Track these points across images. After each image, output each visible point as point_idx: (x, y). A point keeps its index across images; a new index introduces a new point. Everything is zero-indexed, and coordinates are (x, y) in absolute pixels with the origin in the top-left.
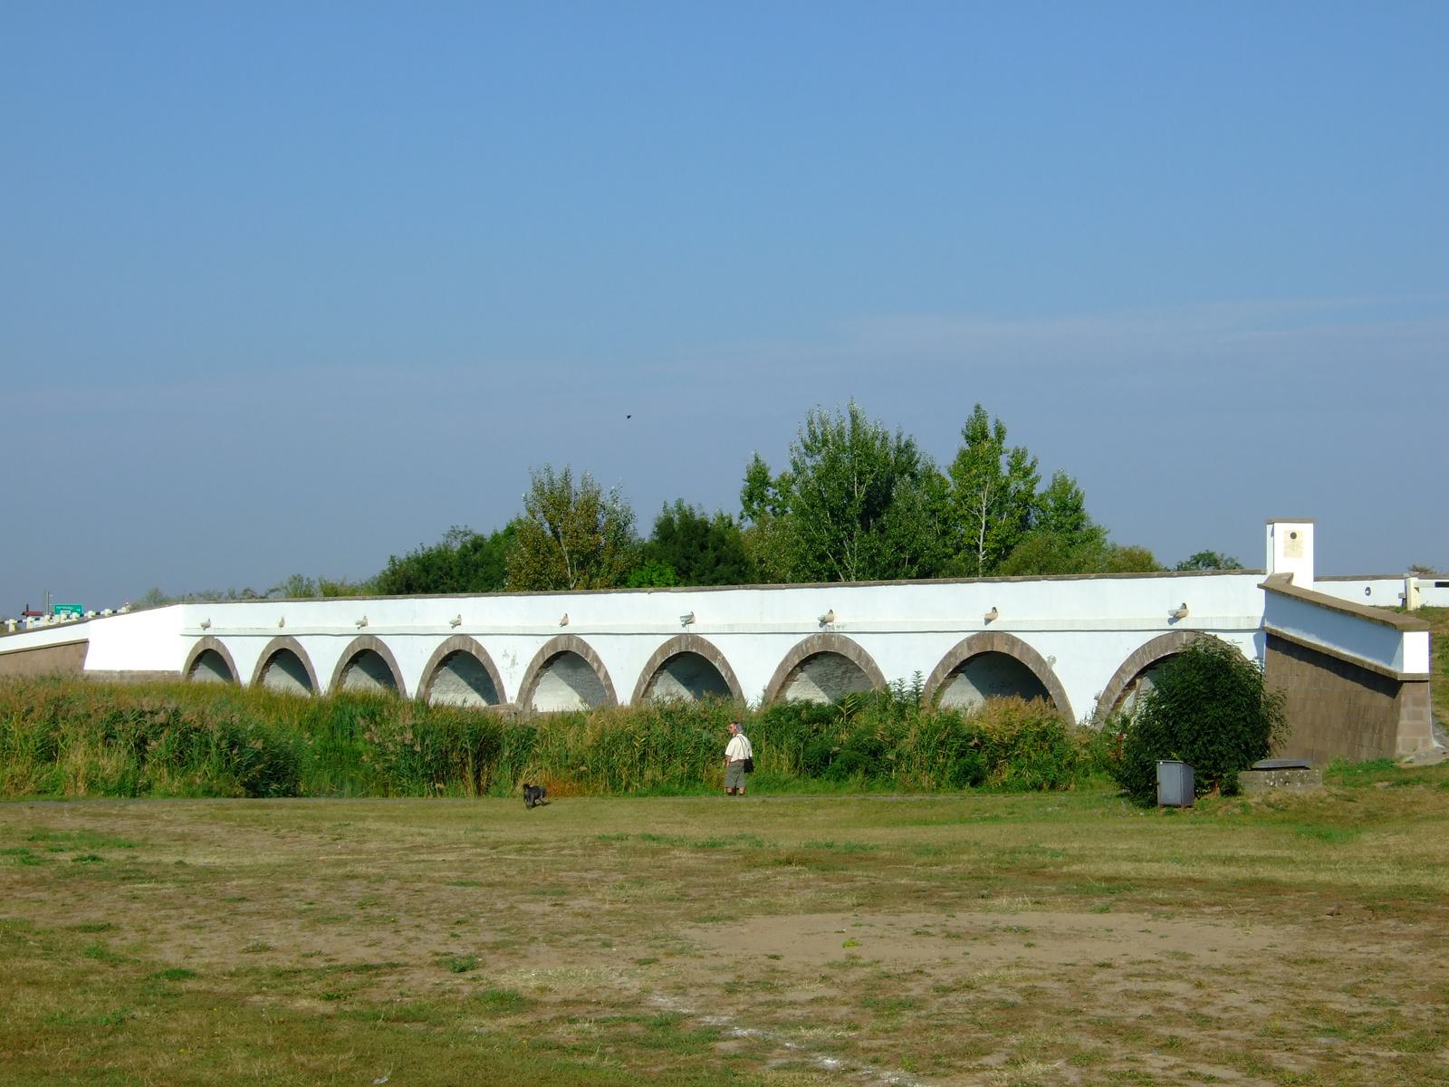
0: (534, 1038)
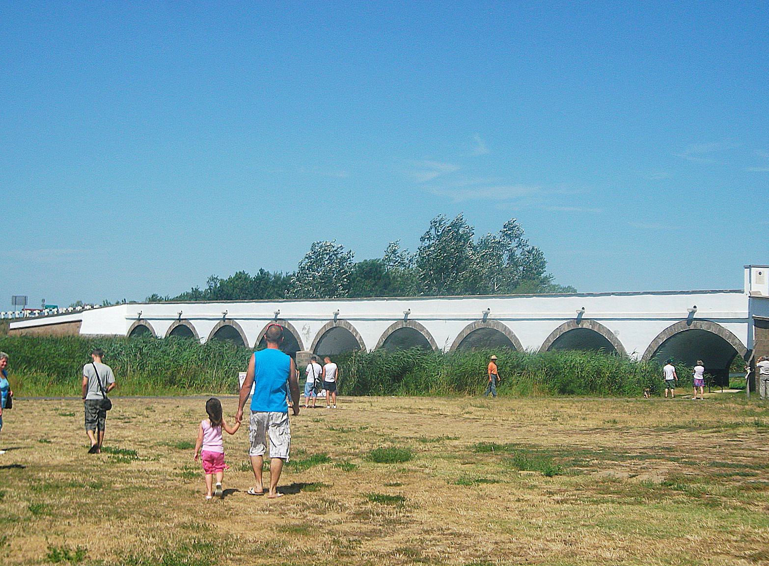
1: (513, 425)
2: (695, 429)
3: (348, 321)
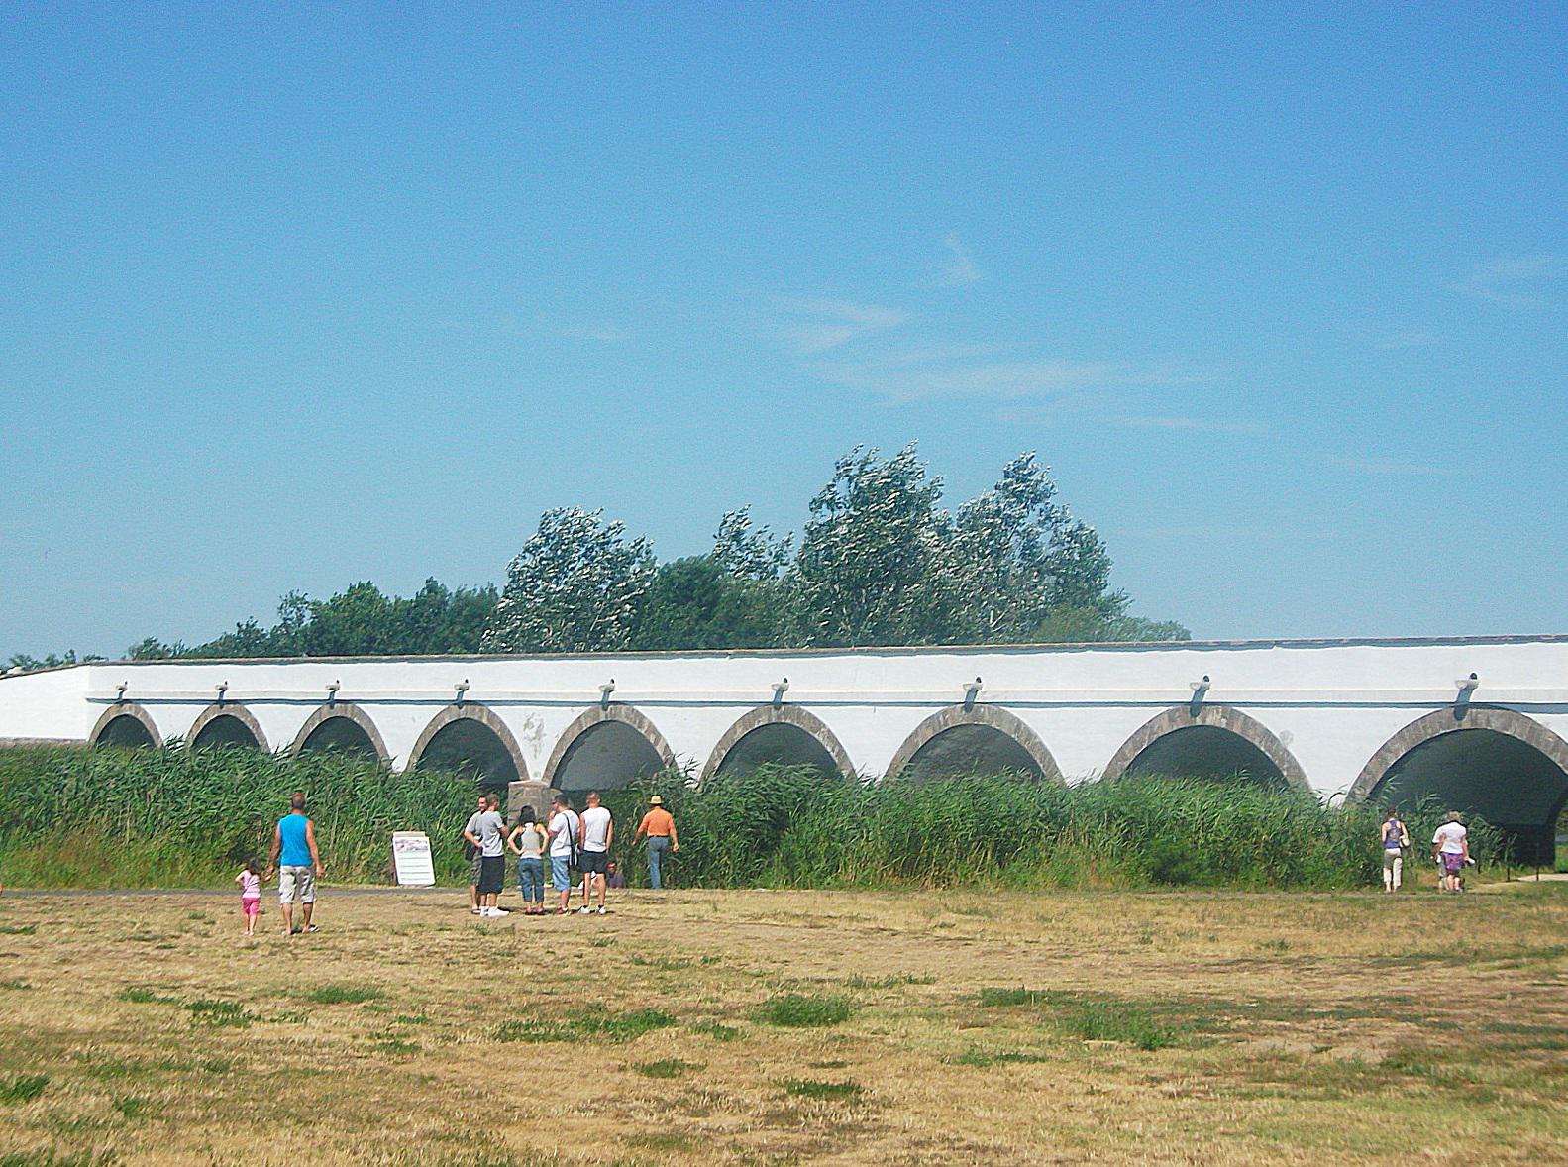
0: (1309, 894)
1: (1049, 953)
2: (1463, 961)
3: (637, 708)
